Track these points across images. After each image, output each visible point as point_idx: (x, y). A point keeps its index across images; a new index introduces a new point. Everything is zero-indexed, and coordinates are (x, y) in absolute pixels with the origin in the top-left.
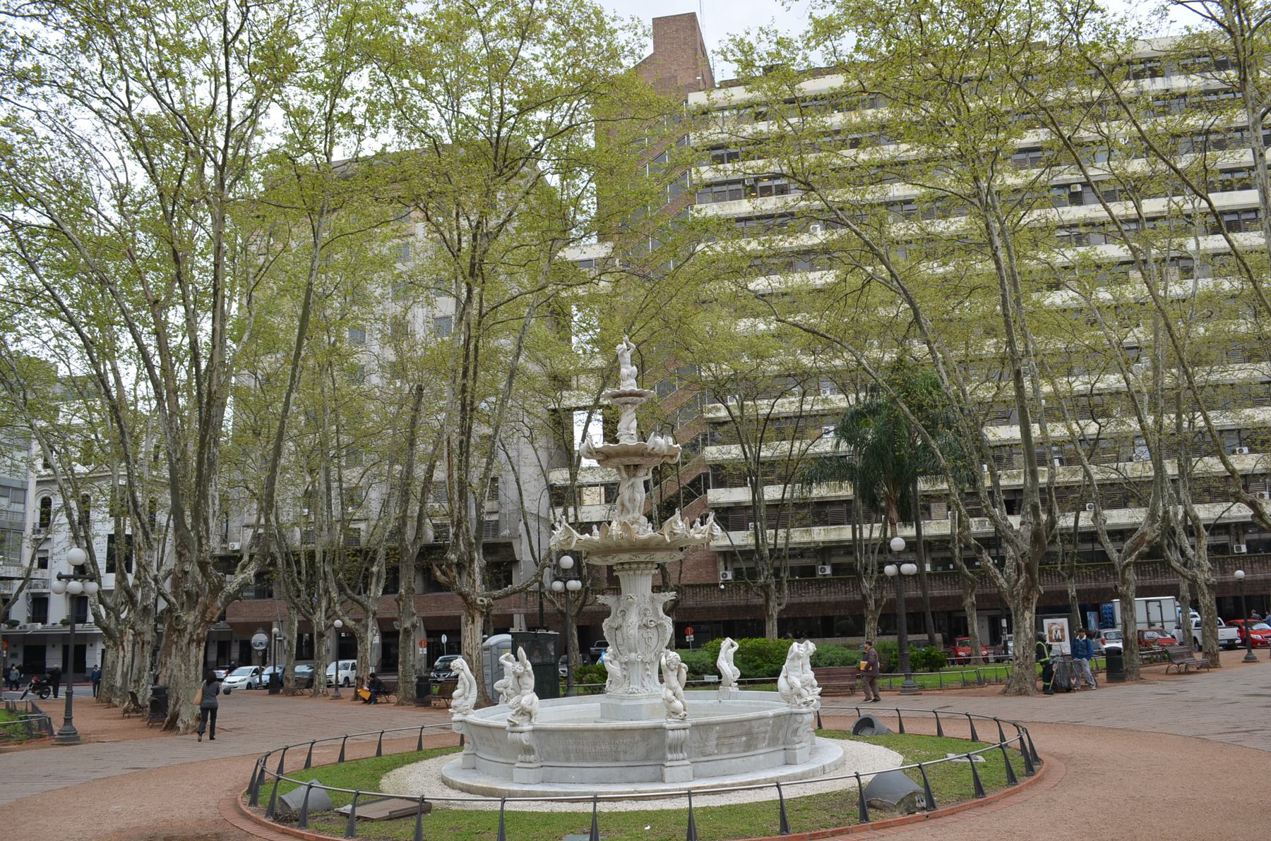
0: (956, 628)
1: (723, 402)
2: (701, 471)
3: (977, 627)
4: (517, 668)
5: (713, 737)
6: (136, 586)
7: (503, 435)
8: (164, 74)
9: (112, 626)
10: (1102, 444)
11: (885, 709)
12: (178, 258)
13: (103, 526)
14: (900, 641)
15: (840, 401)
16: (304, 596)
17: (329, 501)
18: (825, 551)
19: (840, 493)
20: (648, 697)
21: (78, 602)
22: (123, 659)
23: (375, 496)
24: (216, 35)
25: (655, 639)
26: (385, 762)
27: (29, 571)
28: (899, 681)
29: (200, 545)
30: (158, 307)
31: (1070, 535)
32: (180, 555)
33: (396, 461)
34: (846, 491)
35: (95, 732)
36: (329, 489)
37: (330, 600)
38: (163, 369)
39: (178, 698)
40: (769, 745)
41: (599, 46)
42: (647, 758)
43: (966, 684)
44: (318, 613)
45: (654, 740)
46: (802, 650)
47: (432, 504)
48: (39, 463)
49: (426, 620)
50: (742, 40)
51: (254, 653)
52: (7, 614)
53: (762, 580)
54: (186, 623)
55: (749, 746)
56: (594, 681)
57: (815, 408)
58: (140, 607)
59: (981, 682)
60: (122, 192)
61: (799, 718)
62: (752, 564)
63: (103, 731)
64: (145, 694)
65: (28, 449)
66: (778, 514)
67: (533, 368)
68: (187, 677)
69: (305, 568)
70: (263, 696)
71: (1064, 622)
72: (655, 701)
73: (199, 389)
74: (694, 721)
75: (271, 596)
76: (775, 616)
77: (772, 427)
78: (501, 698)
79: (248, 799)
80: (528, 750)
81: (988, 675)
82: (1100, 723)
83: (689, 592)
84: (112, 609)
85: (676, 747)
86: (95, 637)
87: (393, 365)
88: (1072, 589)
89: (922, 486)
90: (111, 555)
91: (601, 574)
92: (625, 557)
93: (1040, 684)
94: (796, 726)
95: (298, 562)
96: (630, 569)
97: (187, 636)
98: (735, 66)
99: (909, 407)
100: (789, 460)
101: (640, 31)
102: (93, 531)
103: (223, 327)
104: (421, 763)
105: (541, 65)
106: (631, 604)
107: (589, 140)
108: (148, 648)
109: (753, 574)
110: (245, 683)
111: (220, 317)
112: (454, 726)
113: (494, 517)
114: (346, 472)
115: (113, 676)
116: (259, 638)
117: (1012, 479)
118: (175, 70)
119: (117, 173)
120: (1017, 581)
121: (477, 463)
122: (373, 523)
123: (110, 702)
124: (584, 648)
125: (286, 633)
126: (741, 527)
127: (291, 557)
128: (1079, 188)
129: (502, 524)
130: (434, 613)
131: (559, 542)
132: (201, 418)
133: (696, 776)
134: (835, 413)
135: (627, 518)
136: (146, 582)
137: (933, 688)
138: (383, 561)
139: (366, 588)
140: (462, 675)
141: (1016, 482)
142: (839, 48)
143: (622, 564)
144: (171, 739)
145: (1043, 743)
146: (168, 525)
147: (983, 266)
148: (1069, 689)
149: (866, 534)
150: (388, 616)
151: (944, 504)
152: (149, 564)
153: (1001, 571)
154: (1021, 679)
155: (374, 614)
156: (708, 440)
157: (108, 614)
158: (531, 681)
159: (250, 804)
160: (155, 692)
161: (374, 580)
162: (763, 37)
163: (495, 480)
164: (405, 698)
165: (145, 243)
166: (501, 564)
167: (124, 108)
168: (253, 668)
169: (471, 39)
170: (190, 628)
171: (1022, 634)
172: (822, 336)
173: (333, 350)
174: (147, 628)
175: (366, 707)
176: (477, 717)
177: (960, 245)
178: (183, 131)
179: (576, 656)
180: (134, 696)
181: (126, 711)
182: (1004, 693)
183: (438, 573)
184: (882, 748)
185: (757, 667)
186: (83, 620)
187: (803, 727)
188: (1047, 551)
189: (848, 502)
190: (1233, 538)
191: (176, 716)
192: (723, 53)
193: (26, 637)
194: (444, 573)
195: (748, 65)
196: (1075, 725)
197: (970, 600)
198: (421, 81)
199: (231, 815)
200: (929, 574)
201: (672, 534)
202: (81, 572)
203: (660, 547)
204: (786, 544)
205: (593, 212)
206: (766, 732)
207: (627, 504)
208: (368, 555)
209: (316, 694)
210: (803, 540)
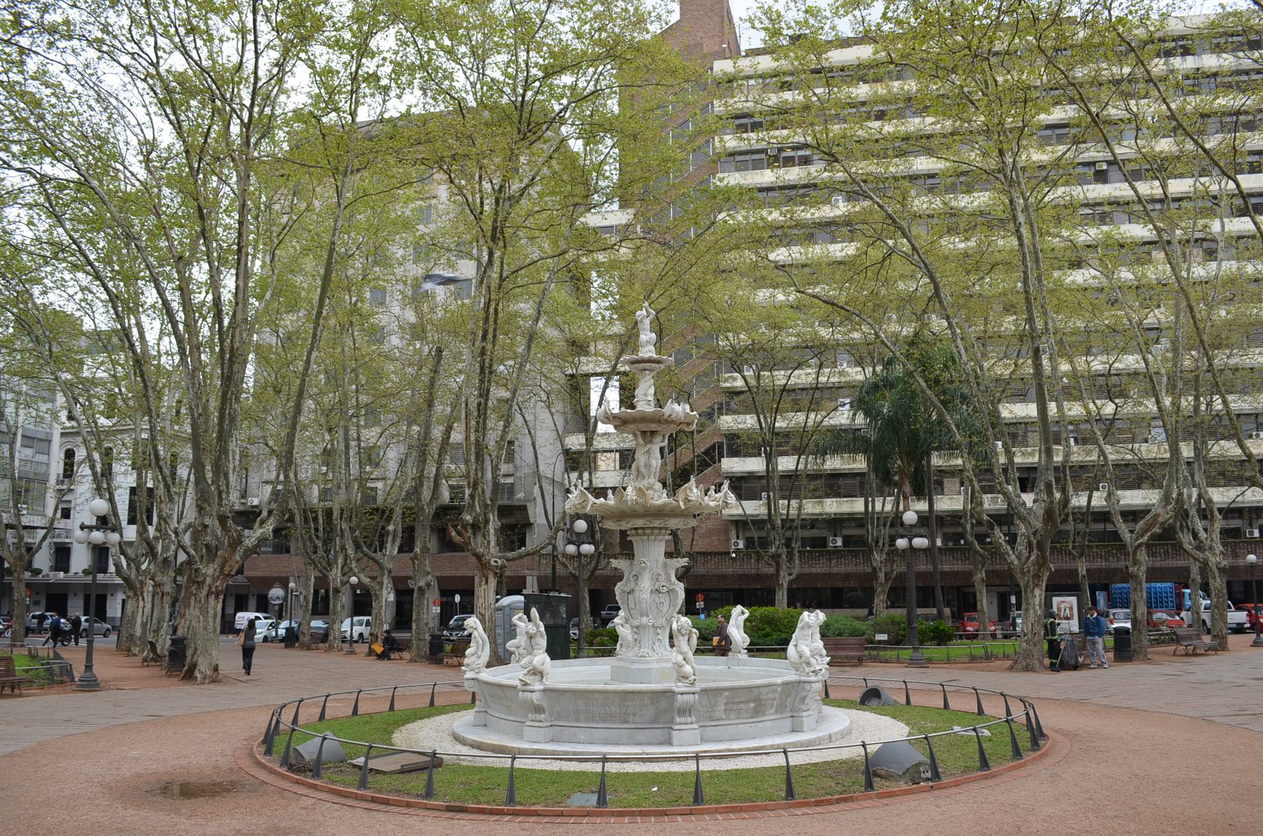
0: (965, 603)
1: (740, 371)
3: (986, 603)
4: (530, 629)
5: (722, 701)
6: (156, 538)
7: (520, 399)
8: (192, 30)
9: (133, 577)
10: (1118, 424)
11: (888, 677)
12: (203, 214)
13: (125, 479)
14: (909, 614)
15: (856, 374)
16: (321, 552)
17: (348, 459)
18: (836, 523)
20: (659, 661)
21: (100, 552)
23: (392, 456)
25: (666, 604)
28: (907, 653)
29: (220, 499)
30: (182, 263)
32: (200, 509)
34: (860, 464)
35: (115, 680)
36: (347, 447)
37: (346, 557)
38: (186, 325)
39: (196, 649)
40: (776, 712)
41: (626, 10)
42: (655, 721)
43: (973, 659)
44: (334, 570)
45: (663, 704)
46: (812, 619)
48: (63, 415)
49: (440, 579)
50: (770, 8)
52: (30, 562)
53: (774, 550)
54: (205, 575)
55: (757, 712)
56: (605, 644)
57: (832, 380)
58: (160, 558)
59: (988, 657)
60: (148, 147)
61: (807, 686)
62: (763, 534)
63: (122, 679)
64: (164, 644)
65: (53, 401)
66: (792, 484)
67: (552, 333)
68: (205, 628)
69: (323, 525)
71: (1073, 600)
72: (664, 665)
74: (704, 686)
75: (288, 551)
76: (785, 586)
80: (539, 709)
81: (995, 651)
83: (700, 559)
84: (133, 560)
85: (685, 711)
87: (413, 326)
88: (1082, 568)
89: (937, 460)
90: (132, 507)
92: (639, 523)
93: (1047, 661)
94: (804, 694)
95: (315, 519)
96: (644, 534)
97: (206, 589)
98: (762, 34)
100: (803, 432)
104: (432, 719)
105: (567, 28)
106: (644, 569)
107: (613, 105)
108: (167, 600)
109: (764, 543)
112: (466, 684)
113: (510, 480)
114: (364, 432)
115: (133, 625)
116: (276, 593)
118: (203, 27)
122: (390, 482)
124: (595, 612)
125: (301, 588)
127: (309, 514)
128: (1105, 167)
129: (517, 487)
133: (704, 740)
134: (851, 386)
135: (642, 484)
136: (166, 534)
138: (399, 520)
139: (382, 546)
142: (868, 18)
143: (636, 529)
144: (188, 688)
145: (1049, 719)
146: (188, 479)
147: (1005, 243)
149: (878, 507)
150: (403, 574)
151: (957, 480)
152: (170, 516)
153: (1013, 548)
154: (1028, 655)
155: (390, 572)
156: (723, 409)
157: (128, 565)
158: (543, 642)
160: (174, 642)
161: (390, 538)
163: (511, 443)
164: (418, 655)
166: (515, 526)
167: (152, 64)
170: (209, 580)
171: (1031, 611)
172: (842, 308)
173: (355, 310)
174: (166, 579)
176: (488, 675)
177: (982, 221)
179: (587, 619)
180: (153, 645)
181: (145, 660)
182: (1011, 668)
183: (454, 534)
184: (888, 718)
185: (766, 636)
186: (105, 571)
187: (810, 695)
189: (862, 475)
190: (1246, 522)
191: (193, 666)
192: (751, 21)
194: (459, 533)
195: (775, 33)
196: (1081, 702)
197: (980, 576)
198: (447, 42)
199: (246, 764)
200: (940, 549)
201: (687, 500)
202: (104, 522)
203: (674, 513)
204: (799, 515)
205: (615, 178)
207: (643, 470)
208: (384, 514)
209: (330, 648)
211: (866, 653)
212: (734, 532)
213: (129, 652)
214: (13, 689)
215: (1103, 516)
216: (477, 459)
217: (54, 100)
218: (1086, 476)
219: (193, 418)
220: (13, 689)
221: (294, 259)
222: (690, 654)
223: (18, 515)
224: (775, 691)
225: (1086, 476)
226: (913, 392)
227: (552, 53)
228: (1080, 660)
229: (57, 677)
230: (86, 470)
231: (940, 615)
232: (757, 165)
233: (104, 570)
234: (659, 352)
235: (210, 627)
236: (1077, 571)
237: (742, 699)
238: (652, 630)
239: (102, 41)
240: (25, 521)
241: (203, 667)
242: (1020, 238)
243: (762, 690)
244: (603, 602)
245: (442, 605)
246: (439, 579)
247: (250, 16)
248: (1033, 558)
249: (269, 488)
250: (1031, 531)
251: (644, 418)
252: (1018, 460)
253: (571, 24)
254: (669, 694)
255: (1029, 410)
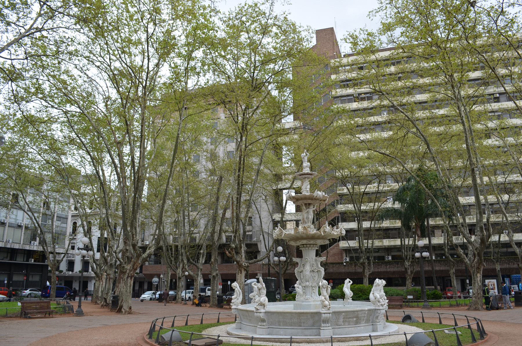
0: (445, 282)
1: (345, 186)
2: (336, 215)
3: (455, 283)
4: (258, 286)
6: (108, 256)
7: (254, 199)
8: (124, 52)
9: (98, 272)
10: (511, 205)
11: (415, 313)
12: (127, 124)
13: (96, 233)
14: (422, 289)
15: (396, 186)
16: (173, 263)
17: (184, 223)
18: (389, 250)
19: (396, 225)
20: (314, 301)
21: (86, 264)
22: (102, 285)
23: (202, 223)
24: (144, 37)
25: (317, 277)
26: (203, 326)
27: (67, 251)
28: (421, 304)
29: (133, 237)
30: (120, 144)
31: (497, 244)
32: (125, 243)
33: (210, 209)
34: (398, 224)
35: (90, 312)
36: (184, 219)
37: (184, 264)
38: (121, 168)
39: (122, 300)
40: (366, 323)
41: (294, 38)
42: (313, 326)
43: (451, 306)
44: (179, 269)
47: (225, 227)
48: (73, 208)
49: (222, 275)
50: (353, 34)
51: (153, 286)
52: (58, 267)
53: (362, 261)
54: (127, 269)
55: (357, 322)
56: (290, 295)
57: (384, 189)
58: (109, 264)
59: (458, 305)
60: (107, 99)
61: (379, 311)
62: (357, 255)
63: (93, 312)
64: (110, 299)
65: (69, 202)
66: (369, 233)
67: (266, 171)
68: (126, 291)
69: (175, 252)
70: (156, 303)
71: (495, 281)
72: (316, 303)
73: (134, 177)
74: (334, 310)
75: (160, 263)
76: (367, 276)
77: (366, 198)
78: (253, 298)
79: (148, 337)
80: (263, 321)
81: (461, 303)
82: (513, 321)
83: (331, 266)
84: (98, 265)
85: (326, 321)
86: (91, 278)
87: (210, 170)
88: (498, 267)
89: (432, 222)
90: (99, 246)
91: (292, 250)
92: (304, 242)
93: (485, 307)
94: (377, 315)
95: (171, 249)
96: (307, 247)
97: (127, 275)
98: (350, 45)
99: (425, 185)
100: (373, 211)
101: (311, 31)
102: (92, 234)
103: (144, 154)
105: (270, 46)
106: (307, 262)
107: (290, 76)
108: (112, 281)
109: (358, 258)
110: (149, 298)
111: (142, 148)
113: (250, 233)
114: (191, 213)
115: (98, 292)
116: (155, 280)
117: (471, 219)
118: (128, 51)
119: (105, 90)
120: (474, 260)
121: (243, 209)
122: (201, 234)
123: (96, 302)
124: (287, 288)
125: (166, 278)
126: (353, 239)
127: (169, 248)
128: (498, 95)
129: (253, 236)
130: (225, 272)
131: (277, 235)
132: (134, 187)
134: (391, 191)
135: (306, 225)
136: (112, 254)
137: (437, 307)
138: (205, 248)
139: (198, 259)
140: (236, 289)
141: (472, 221)
142: (393, 35)
143: (303, 245)
144: (119, 316)
145: (487, 328)
146: (121, 233)
147: (457, 128)
148: (498, 309)
149: (407, 243)
151: (441, 230)
152: (113, 246)
153: (467, 257)
154: (476, 303)
155: (201, 270)
157: (97, 267)
158: (265, 291)
159: (149, 338)
160: (114, 297)
161: (201, 256)
162: (362, 32)
163: (250, 218)
164: (213, 304)
165: (116, 121)
166: (253, 252)
167: (108, 65)
168: (153, 292)
169: (242, 37)
170: (128, 271)
171: (476, 284)
172: (388, 155)
173: (187, 162)
174: (111, 272)
175: (197, 308)
176: (241, 307)
177: (445, 120)
178: (130, 73)
179: (283, 291)
180: (105, 299)
181: (102, 306)
182: (469, 309)
183: (227, 253)
184: (415, 327)
186: (87, 271)
187: (380, 316)
188: (485, 250)
189: (399, 229)
191: (121, 307)
192: (345, 39)
193: (65, 277)
194: (229, 252)
195: (355, 44)
196: (501, 322)
197: (453, 271)
198: (223, 54)
199: (141, 342)
200: (434, 260)
201: (324, 232)
202: (88, 248)
203: (319, 237)
204: (372, 246)
205: (291, 106)
206: (364, 317)
207: (306, 220)
208: (199, 247)
209: (177, 302)
210: (379, 245)
211: (404, 304)
212: (344, 254)
213: (96, 303)
214: (49, 314)
215: (507, 245)
216: (237, 221)
217: (71, 81)
218: (499, 228)
219: (123, 205)
220: (49, 314)
221: (163, 143)
222: (328, 297)
223: (54, 248)
224: (365, 313)
225: (499, 228)
226: (419, 190)
227: (264, 55)
228: (500, 305)
229: (67, 311)
230: (81, 229)
231: (436, 288)
232: (350, 101)
233: (87, 271)
234: (311, 170)
235: (128, 291)
236: (495, 269)
237: (351, 316)
238: (311, 288)
239: (89, 57)
240: (57, 250)
241: (125, 307)
242: (464, 125)
243: (359, 312)
244: (290, 282)
245: (223, 285)
246: (222, 275)
247: (146, 45)
248: (476, 260)
249: (152, 237)
250: (474, 248)
251: (306, 198)
252: (467, 221)
253: (272, 44)
254: (319, 314)
255: (472, 199)
